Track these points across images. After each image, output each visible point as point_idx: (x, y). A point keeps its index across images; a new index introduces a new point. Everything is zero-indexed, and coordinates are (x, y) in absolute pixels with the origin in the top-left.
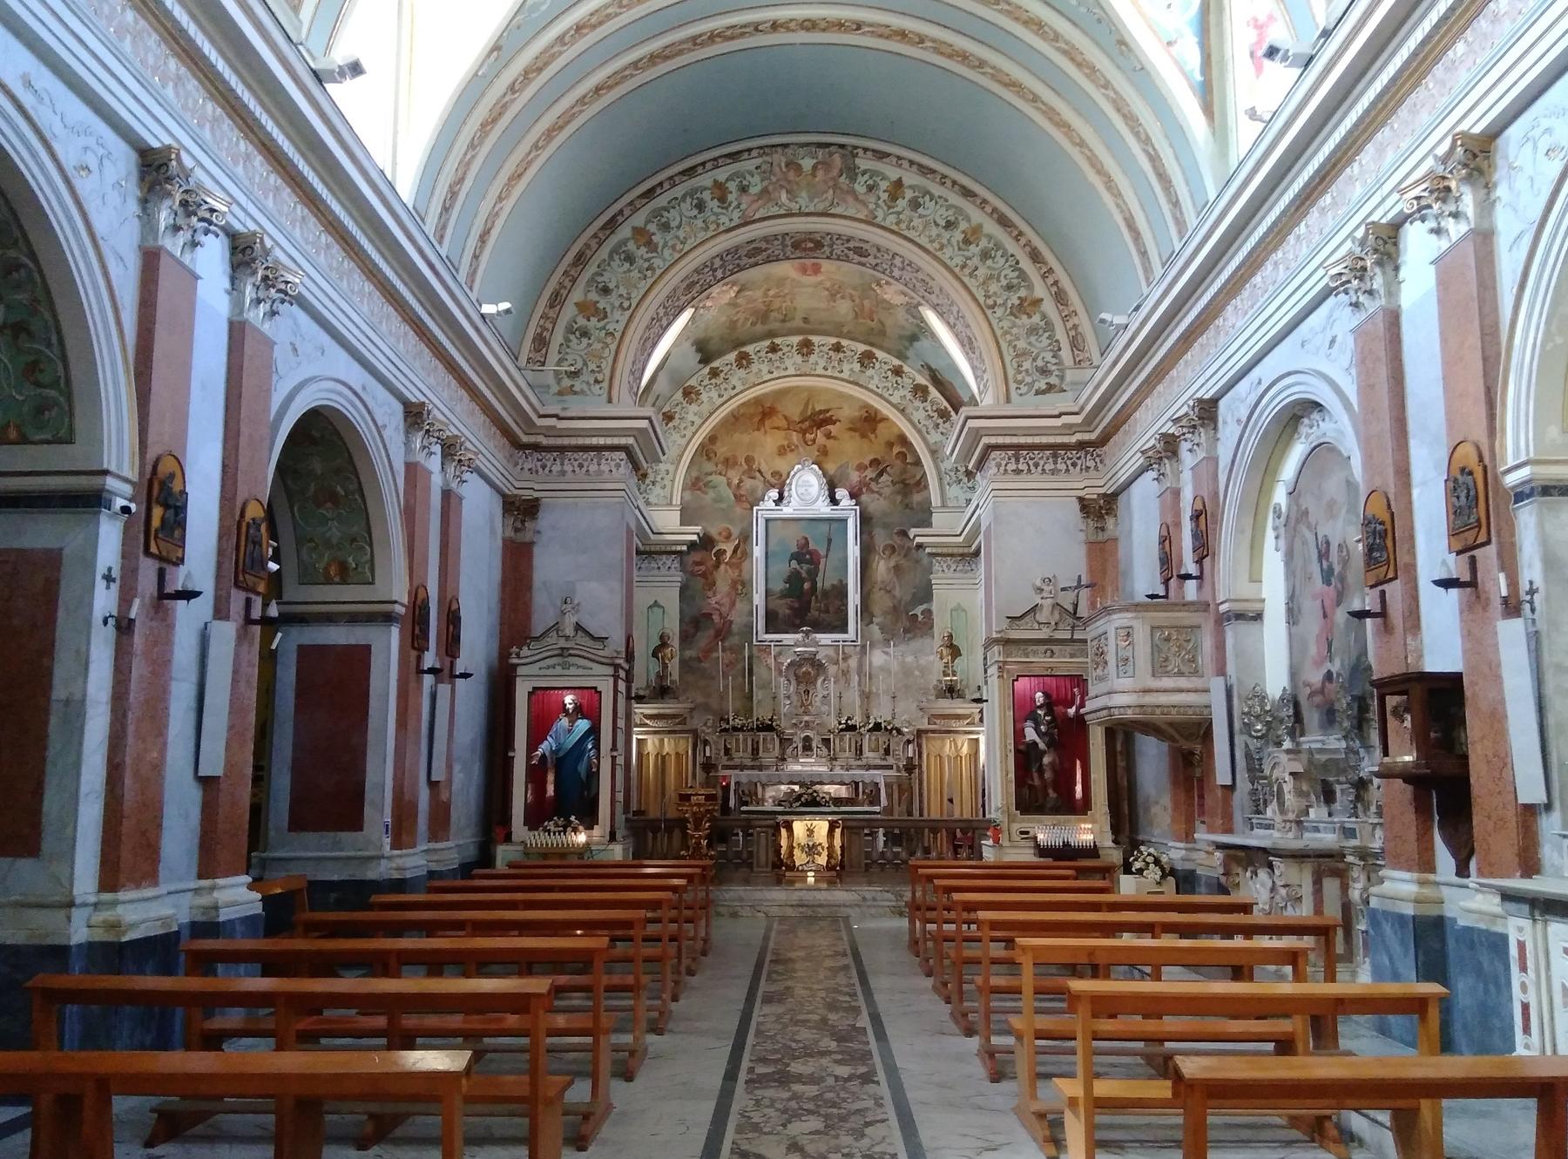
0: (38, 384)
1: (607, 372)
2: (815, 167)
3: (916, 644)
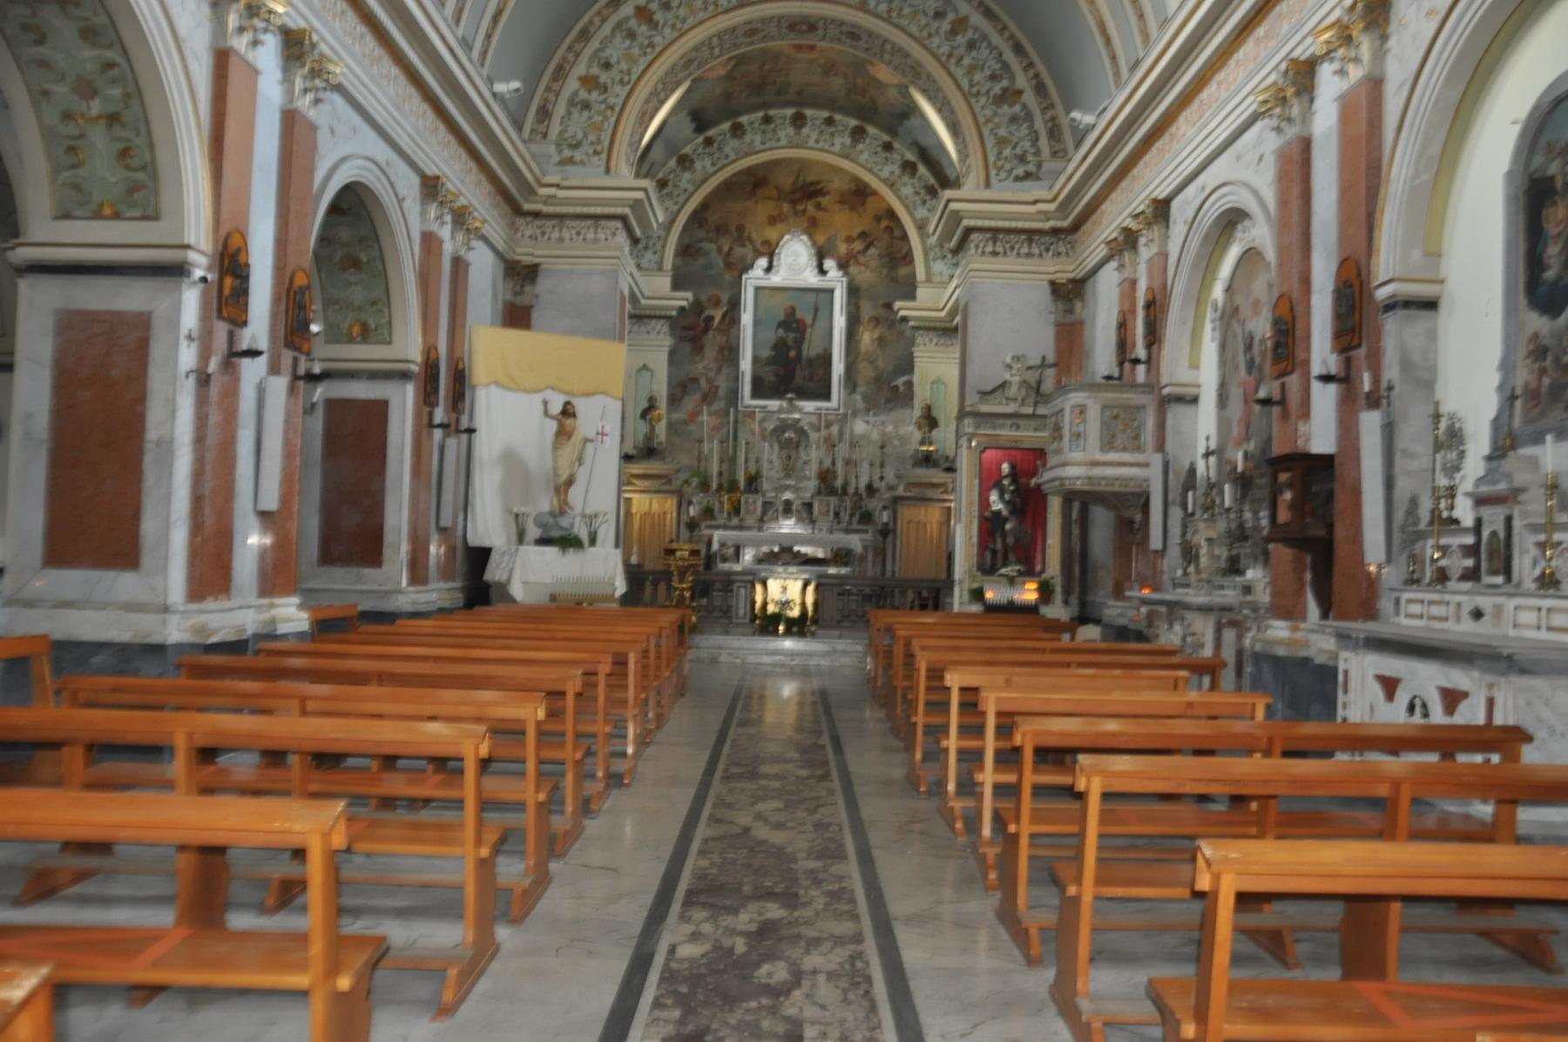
3: (898, 414)
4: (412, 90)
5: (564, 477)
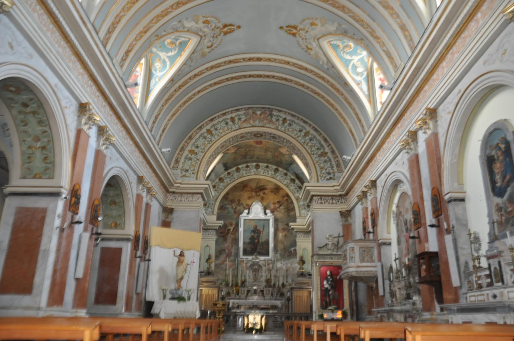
0: (46, 163)
1: (196, 171)
2: (261, 114)
3: (291, 260)
4: (136, 149)
5: (180, 277)
